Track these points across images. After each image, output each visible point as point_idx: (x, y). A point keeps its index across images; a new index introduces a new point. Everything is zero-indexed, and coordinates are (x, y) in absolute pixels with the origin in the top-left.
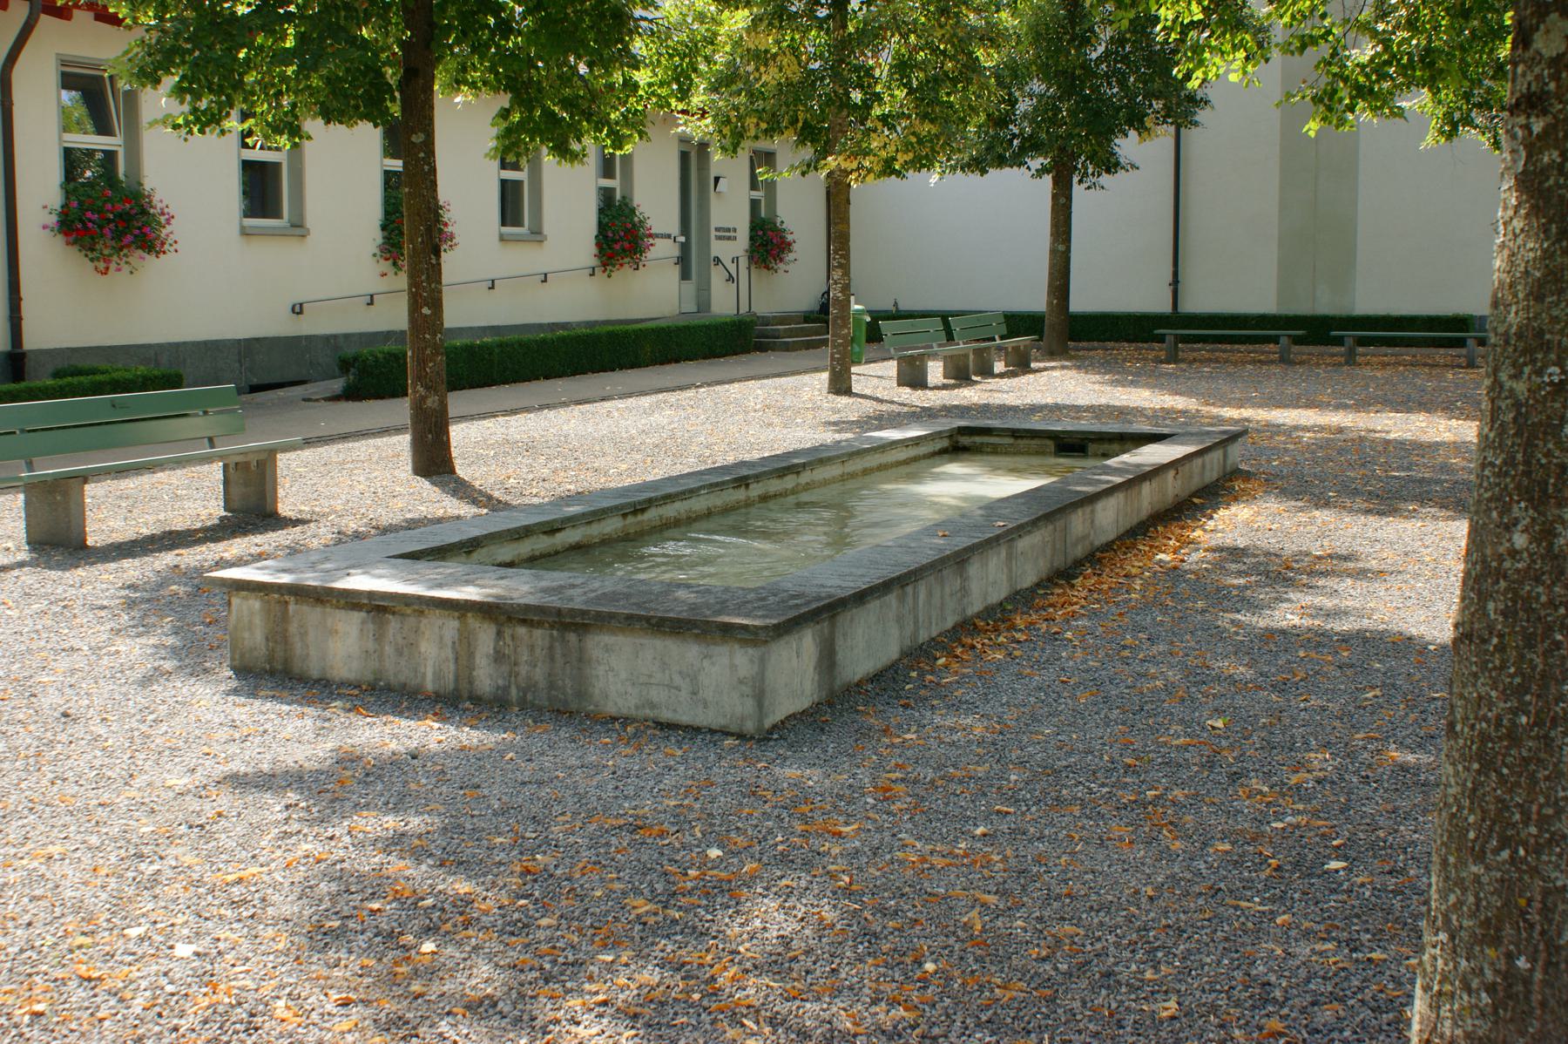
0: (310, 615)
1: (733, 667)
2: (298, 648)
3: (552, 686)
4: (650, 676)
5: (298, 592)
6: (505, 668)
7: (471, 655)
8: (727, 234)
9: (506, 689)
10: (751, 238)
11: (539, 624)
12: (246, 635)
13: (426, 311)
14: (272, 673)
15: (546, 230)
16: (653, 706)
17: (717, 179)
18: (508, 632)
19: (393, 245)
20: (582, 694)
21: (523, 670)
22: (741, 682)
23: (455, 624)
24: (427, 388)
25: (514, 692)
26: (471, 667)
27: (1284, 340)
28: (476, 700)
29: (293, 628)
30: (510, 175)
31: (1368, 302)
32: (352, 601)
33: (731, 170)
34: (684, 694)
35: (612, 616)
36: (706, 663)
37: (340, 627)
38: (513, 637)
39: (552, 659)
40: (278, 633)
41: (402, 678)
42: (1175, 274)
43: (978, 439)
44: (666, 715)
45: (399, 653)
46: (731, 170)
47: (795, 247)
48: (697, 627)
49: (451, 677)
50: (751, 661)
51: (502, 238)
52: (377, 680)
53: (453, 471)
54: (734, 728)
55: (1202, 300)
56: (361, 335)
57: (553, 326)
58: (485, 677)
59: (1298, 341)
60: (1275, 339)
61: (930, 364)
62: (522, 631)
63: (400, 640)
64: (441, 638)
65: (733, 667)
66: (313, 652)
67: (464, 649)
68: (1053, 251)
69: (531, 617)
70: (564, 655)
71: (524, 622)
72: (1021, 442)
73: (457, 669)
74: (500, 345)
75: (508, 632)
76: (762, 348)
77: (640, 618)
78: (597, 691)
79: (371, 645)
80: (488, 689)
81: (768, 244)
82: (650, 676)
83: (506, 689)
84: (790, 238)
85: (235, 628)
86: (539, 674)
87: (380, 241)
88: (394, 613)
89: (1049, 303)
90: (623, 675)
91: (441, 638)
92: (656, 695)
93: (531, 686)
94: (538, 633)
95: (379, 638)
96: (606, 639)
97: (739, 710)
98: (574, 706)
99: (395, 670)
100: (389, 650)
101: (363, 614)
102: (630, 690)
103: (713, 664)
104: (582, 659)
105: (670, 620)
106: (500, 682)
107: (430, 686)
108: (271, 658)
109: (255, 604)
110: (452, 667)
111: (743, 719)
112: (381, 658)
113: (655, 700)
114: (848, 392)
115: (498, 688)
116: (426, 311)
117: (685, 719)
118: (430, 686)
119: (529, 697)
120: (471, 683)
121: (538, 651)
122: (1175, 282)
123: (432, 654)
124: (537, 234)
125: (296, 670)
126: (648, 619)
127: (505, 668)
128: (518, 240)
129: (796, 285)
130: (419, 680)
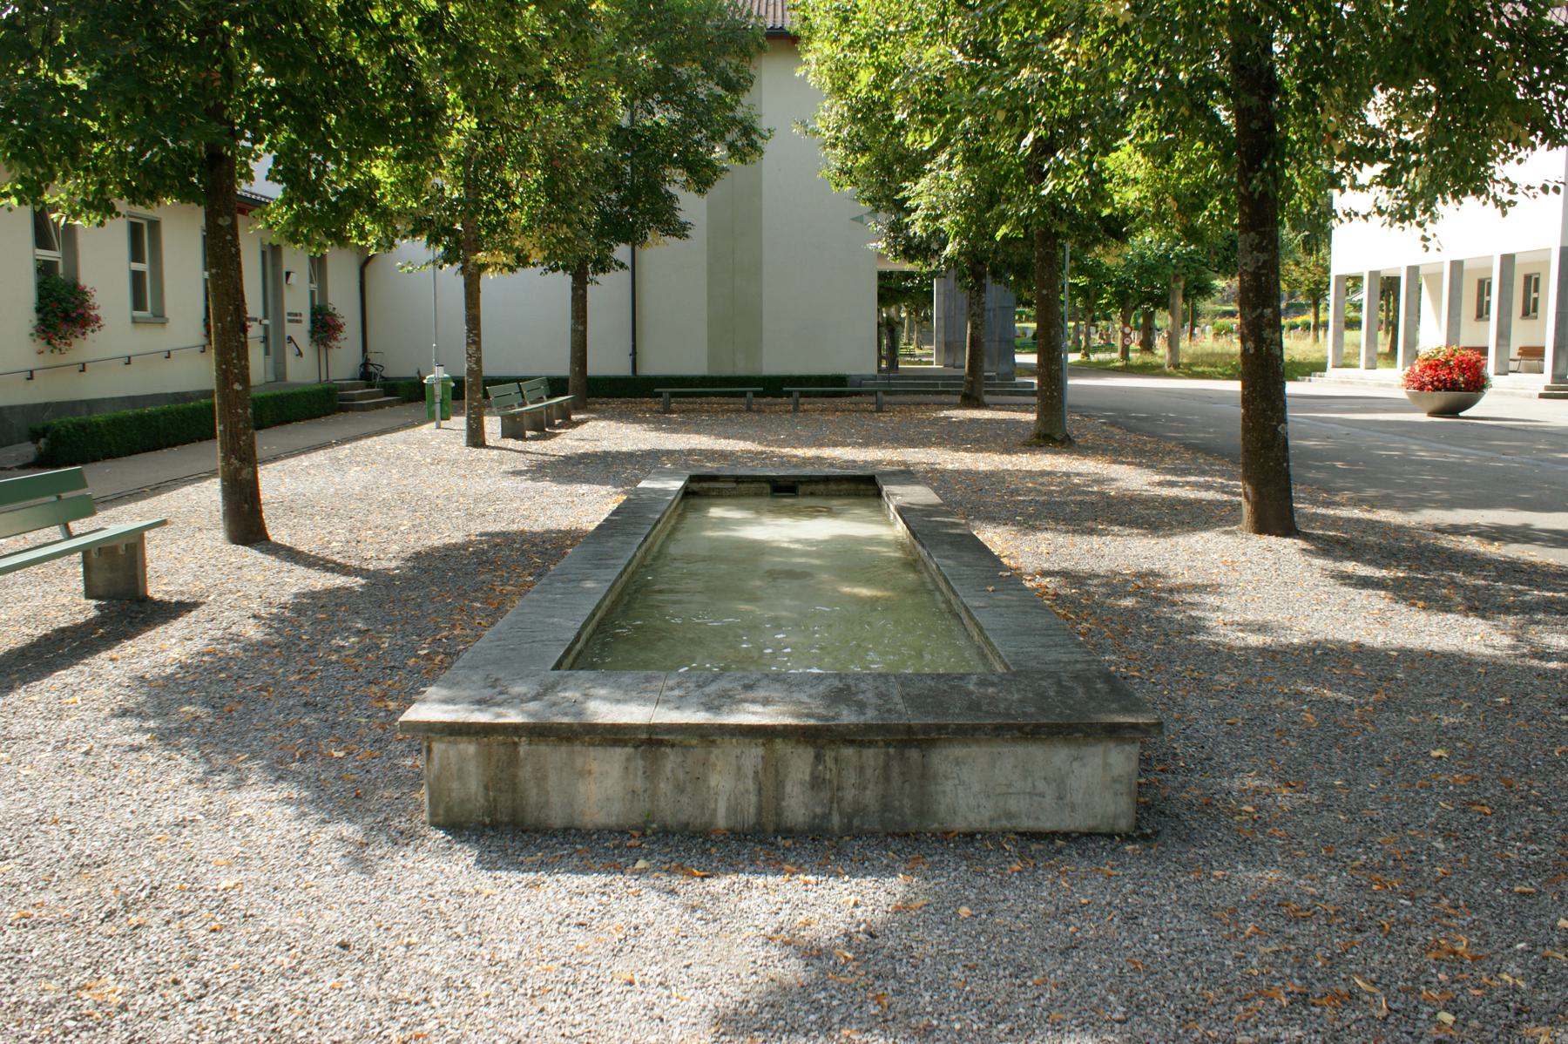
0: (554, 756)
1: (1107, 766)
2: (532, 795)
3: (886, 807)
4: (1010, 785)
5: (539, 732)
6: (825, 795)
7: (780, 785)
8: (295, 318)
9: (826, 816)
10: (312, 322)
11: (871, 744)
12: (455, 785)
13: (237, 387)
14: (494, 826)
15: (168, 314)
16: (1010, 816)
17: (288, 274)
18: (829, 755)
19: (48, 326)
20: (923, 812)
21: (849, 794)
22: (1114, 781)
23: (760, 751)
24: (242, 460)
25: (836, 820)
26: (779, 797)
27: (750, 395)
28: (788, 832)
29: (526, 773)
30: (137, 266)
31: (772, 366)
32: (615, 735)
33: (296, 259)
34: (1049, 800)
35: (976, 728)
36: (1075, 765)
37: (595, 766)
38: (836, 760)
39: (887, 778)
40: (503, 777)
41: (683, 818)
42: (634, 347)
43: (705, 485)
44: (1027, 824)
45: (680, 789)
46: (296, 259)
47: (345, 328)
48: (1078, 730)
49: (752, 810)
50: (1128, 758)
51: (135, 321)
52: (647, 823)
53: (267, 538)
54: (1105, 829)
55: (653, 366)
56: (23, 407)
57: (132, 401)
58: (797, 806)
59: (756, 395)
60: (743, 395)
61: (486, 419)
62: (848, 752)
63: (681, 776)
64: (739, 768)
65: (1107, 766)
66: (555, 799)
67: (771, 781)
68: (574, 331)
69: (872, 737)
70: (903, 774)
71: (852, 742)
72: (743, 486)
73: (760, 801)
74: (164, 413)
75: (829, 755)
76: (345, 409)
77: (1010, 727)
78: (943, 807)
79: (639, 784)
80: (801, 819)
81: (324, 326)
82: (1010, 785)
83: (826, 816)
84: (341, 321)
85: (438, 778)
86: (870, 797)
87: (35, 322)
88: (673, 746)
89: (572, 370)
90: (976, 788)
91: (739, 768)
92: (1013, 804)
93: (860, 810)
94: (869, 752)
95: (651, 775)
96: (958, 751)
97: (1111, 809)
98: (913, 827)
99: (672, 806)
100: (664, 787)
101: (629, 750)
102: (983, 802)
103: (1084, 765)
104: (926, 775)
105: (1044, 725)
106: (818, 810)
107: (721, 822)
108: (491, 809)
109: (469, 748)
110: (753, 799)
111: (1115, 817)
112: (654, 797)
113: (1014, 809)
114: (482, 445)
115: (815, 816)
116: (237, 387)
117: (1048, 825)
118: (721, 822)
119: (856, 822)
120: (778, 814)
121: (869, 772)
122: (634, 353)
123: (727, 789)
124: (159, 317)
125: (531, 817)
126: (1020, 728)
127: (825, 795)
128: (145, 322)
129: (344, 361)
130: (707, 818)
